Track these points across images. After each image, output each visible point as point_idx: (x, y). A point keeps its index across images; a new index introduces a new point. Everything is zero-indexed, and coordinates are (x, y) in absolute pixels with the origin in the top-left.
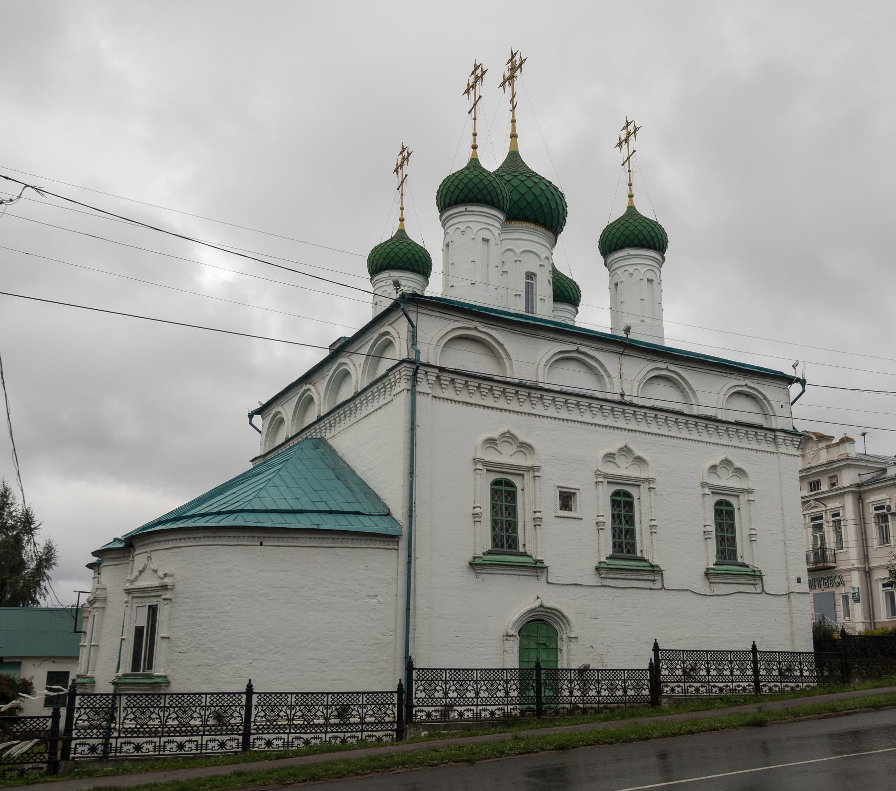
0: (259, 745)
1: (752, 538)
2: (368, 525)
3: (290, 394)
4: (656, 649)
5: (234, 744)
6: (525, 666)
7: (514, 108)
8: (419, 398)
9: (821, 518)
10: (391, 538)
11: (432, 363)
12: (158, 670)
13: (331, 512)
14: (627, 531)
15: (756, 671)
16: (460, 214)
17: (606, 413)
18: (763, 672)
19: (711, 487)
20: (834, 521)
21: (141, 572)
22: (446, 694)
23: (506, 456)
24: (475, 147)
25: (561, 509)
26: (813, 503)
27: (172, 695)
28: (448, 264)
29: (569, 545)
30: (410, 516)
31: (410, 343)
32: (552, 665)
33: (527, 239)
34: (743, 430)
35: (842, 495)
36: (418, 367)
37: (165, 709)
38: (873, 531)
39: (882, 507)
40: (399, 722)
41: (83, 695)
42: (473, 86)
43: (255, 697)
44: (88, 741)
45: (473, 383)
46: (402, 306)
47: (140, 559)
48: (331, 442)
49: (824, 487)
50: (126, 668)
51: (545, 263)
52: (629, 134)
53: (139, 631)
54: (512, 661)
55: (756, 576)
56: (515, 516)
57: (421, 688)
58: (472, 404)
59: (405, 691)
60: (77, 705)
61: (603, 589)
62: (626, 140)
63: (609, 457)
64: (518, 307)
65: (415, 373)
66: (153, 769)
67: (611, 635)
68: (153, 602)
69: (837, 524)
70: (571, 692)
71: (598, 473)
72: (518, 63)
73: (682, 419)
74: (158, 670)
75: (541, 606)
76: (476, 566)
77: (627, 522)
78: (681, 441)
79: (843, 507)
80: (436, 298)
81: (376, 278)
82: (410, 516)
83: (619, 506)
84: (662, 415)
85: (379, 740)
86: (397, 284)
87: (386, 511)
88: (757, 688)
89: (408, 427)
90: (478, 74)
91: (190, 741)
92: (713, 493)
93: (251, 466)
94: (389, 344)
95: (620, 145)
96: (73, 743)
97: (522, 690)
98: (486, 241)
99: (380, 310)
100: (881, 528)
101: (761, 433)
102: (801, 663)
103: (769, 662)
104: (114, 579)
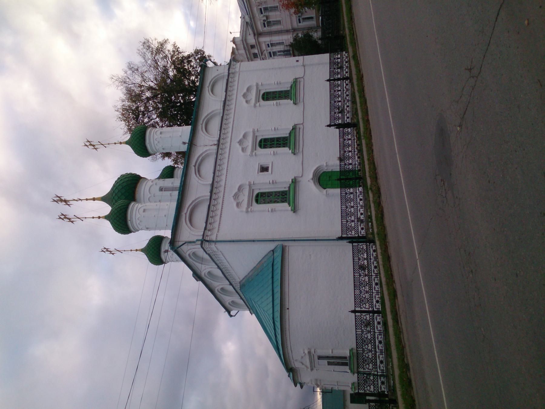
0: (378, 306)
1: (279, 83)
2: (278, 260)
3: (220, 299)
4: (330, 126)
5: (378, 318)
6: (339, 186)
7: (80, 200)
8: (218, 239)
9: (270, 53)
10: (283, 249)
11: (202, 233)
12: (347, 353)
13: (273, 277)
14: (277, 141)
15: (339, 79)
16: (132, 223)
17: (228, 117)
18: (339, 76)
19: (256, 103)
20: (272, 46)
21: (303, 364)
22: (352, 221)
23: (245, 197)
24: (121, 143)
25: (268, 171)
26: (263, 56)
27: (357, 348)
28: (155, 229)
29: (284, 168)
30: (273, 241)
31: (194, 244)
32: (339, 174)
33: (143, 190)
34: (229, 89)
35: (259, 43)
36: (205, 240)
37: (363, 351)
38: (275, 28)
39: (264, 24)
40: (366, 242)
41: (359, 389)
42: (69, 219)
43: (357, 309)
44: (379, 386)
45: (211, 214)
46: (176, 248)
47: (296, 365)
48: (241, 279)
49: (256, 51)
50: (347, 368)
51: (154, 182)
52: (91, 145)
53: (329, 364)
54: (337, 191)
55: (296, 82)
56: (272, 192)
57: (367, 366)
58: (221, 214)
59: (352, 240)
60: (363, 392)
61: (304, 152)
62: (94, 146)
63: (243, 150)
64: (176, 194)
65: (207, 241)
66: (390, 345)
67: (324, 148)
68: (316, 358)
69: (272, 45)
70: (350, 164)
71: (251, 155)
72: (58, 198)
73: (225, 117)
74: (347, 353)
75: (312, 179)
76: (294, 210)
77: (273, 141)
78: (235, 117)
79: (265, 42)
80: (172, 233)
81: (164, 260)
82: (273, 241)
83: (266, 145)
84: (224, 126)
85: (374, 251)
86: (167, 251)
87: (272, 252)
88: (347, 79)
89: (232, 243)
90: (64, 217)
91: (379, 358)
92: (259, 102)
93: (254, 315)
94: (194, 254)
95: (96, 149)
96: (375, 310)
97: (350, 187)
98: (144, 211)
99: (180, 259)
100: (274, 24)
101: (230, 80)
102: (335, 59)
103: (335, 74)
104: (306, 377)
